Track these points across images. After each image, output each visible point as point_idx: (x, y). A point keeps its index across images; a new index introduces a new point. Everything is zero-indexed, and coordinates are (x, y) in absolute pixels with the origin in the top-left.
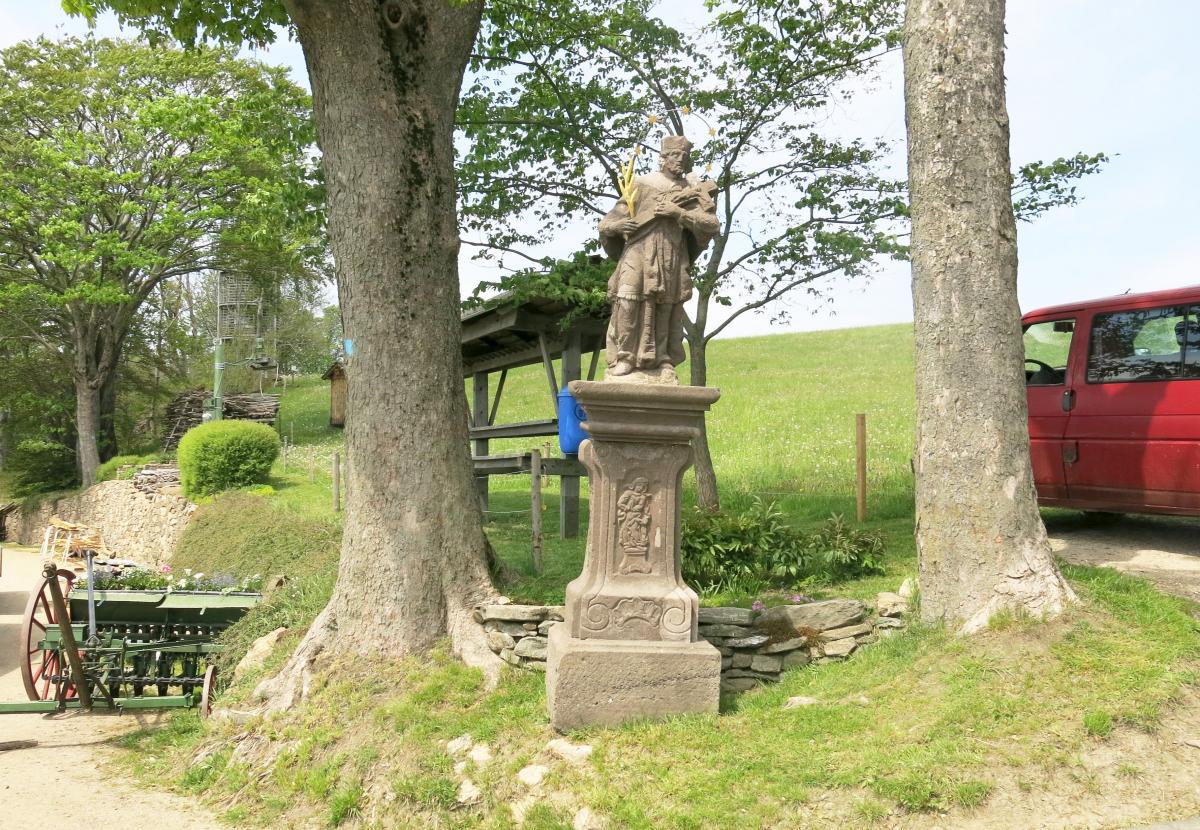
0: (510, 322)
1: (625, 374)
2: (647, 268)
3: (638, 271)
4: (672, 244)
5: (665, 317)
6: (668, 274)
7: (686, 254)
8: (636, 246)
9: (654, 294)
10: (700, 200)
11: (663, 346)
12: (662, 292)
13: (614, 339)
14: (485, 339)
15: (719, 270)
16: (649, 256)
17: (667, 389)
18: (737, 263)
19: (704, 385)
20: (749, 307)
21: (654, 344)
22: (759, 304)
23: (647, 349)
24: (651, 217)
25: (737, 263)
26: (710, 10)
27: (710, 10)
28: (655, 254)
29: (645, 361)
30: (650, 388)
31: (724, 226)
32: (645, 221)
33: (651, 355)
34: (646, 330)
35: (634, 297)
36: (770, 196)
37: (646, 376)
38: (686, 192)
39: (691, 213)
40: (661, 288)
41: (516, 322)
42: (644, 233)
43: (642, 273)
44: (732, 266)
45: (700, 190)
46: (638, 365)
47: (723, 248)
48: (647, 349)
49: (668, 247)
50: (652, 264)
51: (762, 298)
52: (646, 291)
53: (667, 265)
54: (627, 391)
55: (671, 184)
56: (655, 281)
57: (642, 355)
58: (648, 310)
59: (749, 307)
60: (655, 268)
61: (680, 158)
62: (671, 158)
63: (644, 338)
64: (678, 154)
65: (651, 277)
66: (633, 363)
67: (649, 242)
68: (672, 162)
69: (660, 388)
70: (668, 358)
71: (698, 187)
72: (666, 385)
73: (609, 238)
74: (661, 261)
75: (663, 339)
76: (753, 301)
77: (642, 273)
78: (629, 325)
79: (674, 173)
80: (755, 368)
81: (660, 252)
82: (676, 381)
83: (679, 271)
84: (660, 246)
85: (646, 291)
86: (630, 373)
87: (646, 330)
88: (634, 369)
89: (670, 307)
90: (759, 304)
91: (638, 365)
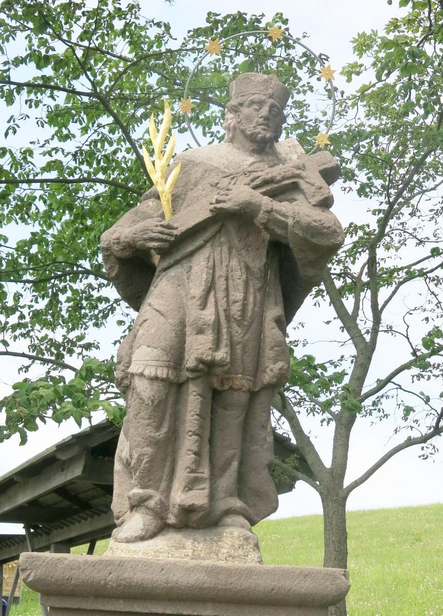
0: (76, 471)
1: (142, 538)
2: (194, 313)
3: (173, 320)
4: (248, 268)
5: (232, 419)
6: (237, 330)
7: (276, 292)
8: (172, 272)
9: (207, 368)
10: (303, 185)
11: (228, 480)
12: (221, 364)
13: (127, 464)
14: (61, 491)
15: (365, 390)
16: (197, 289)
17: (228, 571)
18: (389, 380)
19: (19, 598)
20: (410, 442)
21: (205, 472)
22: (424, 439)
23: (191, 485)
24: (205, 215)
25: (389, 380)
26: (349, 80)
27: (349, 80)
28: (210, 287)
29: (187, 511)
30: (191, 570)
31: (364, 273)
32: (191, 223)
33: (198, 497)
34: (188, 444)
35: (162, 373)
36: (436, 290)
37: (189, 543)
38: (277, 172)
39: (282, 207)
40: (222, 354)
41: (83, 472)
42: (190, 248)
43: (182, 324)
44: (382, 384)
45: (303, 167)
46: (172, 520)
47: (370, 359)
48: (191, 485)
49: (239, 276)
50: (203, 306)
51: (425, 431)
52: (190, 361)
53: (236, 309)
54: (138, 577)
55: (247, 160)
56: (207, 339)
57: (179, 497)
58: (193, 401)
59: (410, 442)
60: (209, 314)
61: (265, 111)
62: (245, 111)
63: (185, 459)
64: (261, 103)
65: (200, 331)
66: (160, 514)
67: (200, 265)
68: (249, 119)
69: (213, 571)
70: (237, 503)
71: (300, 162)
72: (230, 564)
73: (122, 261)
74: (222, 303)
75: (228, 464)
76: (415, 434)
77: (182, 324)
78: (150, 432)
79: (252, 138)
80: (419, 540)
81: (221, 284)
82: (253, 556)
83: (261, 324)
84: (220, 272)
85: (190, 361)
86: (153, 535)
87: (188, 444)
88: (162, 528)
89: (243, 398)
90: (424, 439)
91: (172, 520)
